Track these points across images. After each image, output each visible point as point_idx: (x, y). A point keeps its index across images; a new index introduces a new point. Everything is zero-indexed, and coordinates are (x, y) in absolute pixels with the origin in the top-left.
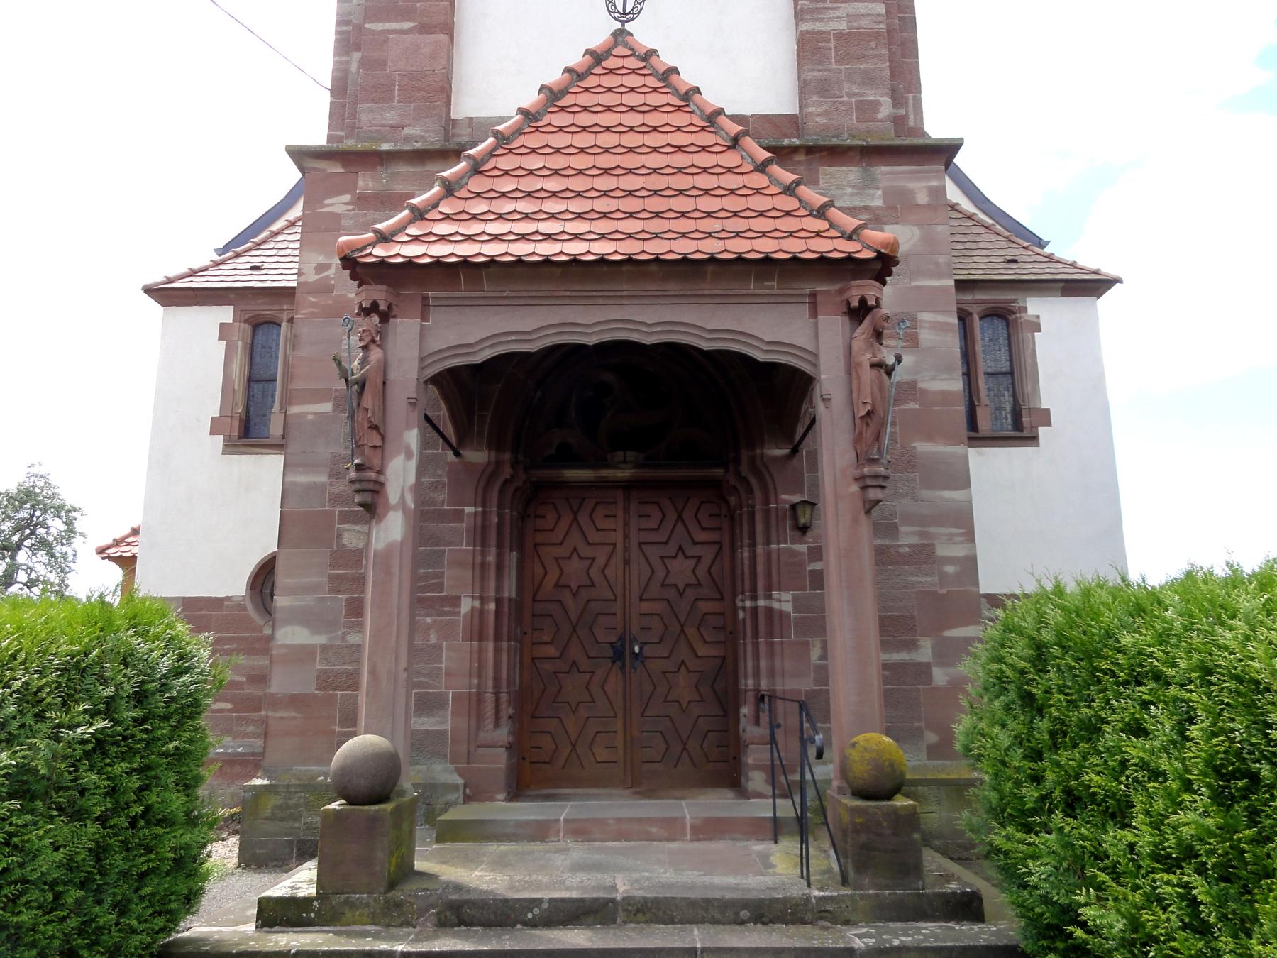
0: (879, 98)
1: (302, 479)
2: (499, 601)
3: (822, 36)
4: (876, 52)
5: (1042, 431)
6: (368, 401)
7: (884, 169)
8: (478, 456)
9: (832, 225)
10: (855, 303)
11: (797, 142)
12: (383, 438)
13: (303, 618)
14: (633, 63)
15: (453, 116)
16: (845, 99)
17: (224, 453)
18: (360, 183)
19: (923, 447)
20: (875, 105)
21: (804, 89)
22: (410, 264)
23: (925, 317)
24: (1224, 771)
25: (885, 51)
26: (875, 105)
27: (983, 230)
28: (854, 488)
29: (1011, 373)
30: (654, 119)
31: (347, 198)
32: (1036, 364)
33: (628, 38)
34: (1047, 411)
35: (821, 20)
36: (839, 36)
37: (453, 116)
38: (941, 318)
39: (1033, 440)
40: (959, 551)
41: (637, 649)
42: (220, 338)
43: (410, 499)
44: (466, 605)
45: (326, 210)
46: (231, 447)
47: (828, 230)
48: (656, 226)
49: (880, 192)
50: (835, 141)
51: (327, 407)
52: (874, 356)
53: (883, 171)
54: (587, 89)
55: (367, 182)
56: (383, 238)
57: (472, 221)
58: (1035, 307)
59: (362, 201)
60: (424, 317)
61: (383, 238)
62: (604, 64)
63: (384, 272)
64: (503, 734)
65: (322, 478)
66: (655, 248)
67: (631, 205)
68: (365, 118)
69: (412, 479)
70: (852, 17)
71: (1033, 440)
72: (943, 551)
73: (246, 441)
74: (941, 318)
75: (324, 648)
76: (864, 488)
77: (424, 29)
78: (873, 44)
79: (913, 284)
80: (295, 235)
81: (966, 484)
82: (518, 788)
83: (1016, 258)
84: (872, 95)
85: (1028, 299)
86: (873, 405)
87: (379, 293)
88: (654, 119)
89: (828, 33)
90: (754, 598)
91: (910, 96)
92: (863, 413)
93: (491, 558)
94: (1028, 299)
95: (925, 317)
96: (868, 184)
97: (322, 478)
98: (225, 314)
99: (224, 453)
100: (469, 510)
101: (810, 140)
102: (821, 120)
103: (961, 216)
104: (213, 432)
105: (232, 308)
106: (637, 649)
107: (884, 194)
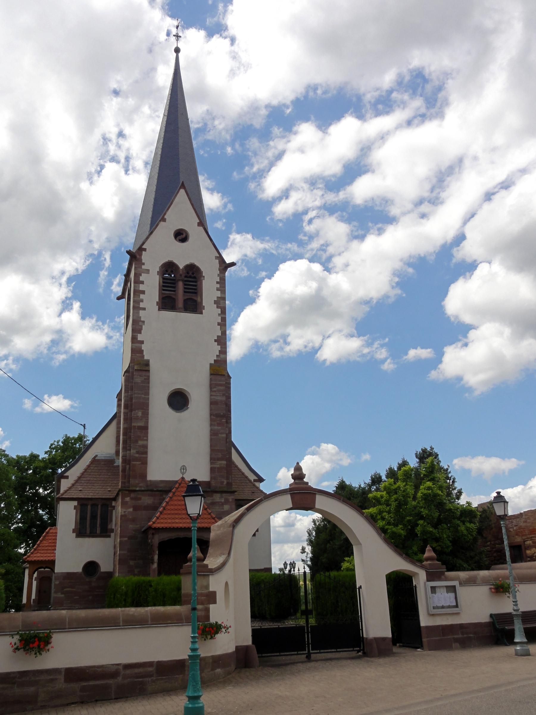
3: (215, 468)
7: (225, 494)
17: (76, 538)
18: (132, 495)
20: (223, 482)
22: (159, 528)
24: (13, 522)
31: (129, 498)
36: (218, 468)
42: (74, 509)
49: (223, 499)
51: (126, 539)
53: (224, 495)
55: (133, 495)
59: (132, 499)
61: (154, 523)
68: (132, 481)
77: (143, 463)
80: (305, 655)
89: (216, 467)
91: (230, 476)
98: (75, 503)
99: (76, 538)
102: (214, 485)
103: (244, 477)
104: (73, 532)
105: (77, 502)
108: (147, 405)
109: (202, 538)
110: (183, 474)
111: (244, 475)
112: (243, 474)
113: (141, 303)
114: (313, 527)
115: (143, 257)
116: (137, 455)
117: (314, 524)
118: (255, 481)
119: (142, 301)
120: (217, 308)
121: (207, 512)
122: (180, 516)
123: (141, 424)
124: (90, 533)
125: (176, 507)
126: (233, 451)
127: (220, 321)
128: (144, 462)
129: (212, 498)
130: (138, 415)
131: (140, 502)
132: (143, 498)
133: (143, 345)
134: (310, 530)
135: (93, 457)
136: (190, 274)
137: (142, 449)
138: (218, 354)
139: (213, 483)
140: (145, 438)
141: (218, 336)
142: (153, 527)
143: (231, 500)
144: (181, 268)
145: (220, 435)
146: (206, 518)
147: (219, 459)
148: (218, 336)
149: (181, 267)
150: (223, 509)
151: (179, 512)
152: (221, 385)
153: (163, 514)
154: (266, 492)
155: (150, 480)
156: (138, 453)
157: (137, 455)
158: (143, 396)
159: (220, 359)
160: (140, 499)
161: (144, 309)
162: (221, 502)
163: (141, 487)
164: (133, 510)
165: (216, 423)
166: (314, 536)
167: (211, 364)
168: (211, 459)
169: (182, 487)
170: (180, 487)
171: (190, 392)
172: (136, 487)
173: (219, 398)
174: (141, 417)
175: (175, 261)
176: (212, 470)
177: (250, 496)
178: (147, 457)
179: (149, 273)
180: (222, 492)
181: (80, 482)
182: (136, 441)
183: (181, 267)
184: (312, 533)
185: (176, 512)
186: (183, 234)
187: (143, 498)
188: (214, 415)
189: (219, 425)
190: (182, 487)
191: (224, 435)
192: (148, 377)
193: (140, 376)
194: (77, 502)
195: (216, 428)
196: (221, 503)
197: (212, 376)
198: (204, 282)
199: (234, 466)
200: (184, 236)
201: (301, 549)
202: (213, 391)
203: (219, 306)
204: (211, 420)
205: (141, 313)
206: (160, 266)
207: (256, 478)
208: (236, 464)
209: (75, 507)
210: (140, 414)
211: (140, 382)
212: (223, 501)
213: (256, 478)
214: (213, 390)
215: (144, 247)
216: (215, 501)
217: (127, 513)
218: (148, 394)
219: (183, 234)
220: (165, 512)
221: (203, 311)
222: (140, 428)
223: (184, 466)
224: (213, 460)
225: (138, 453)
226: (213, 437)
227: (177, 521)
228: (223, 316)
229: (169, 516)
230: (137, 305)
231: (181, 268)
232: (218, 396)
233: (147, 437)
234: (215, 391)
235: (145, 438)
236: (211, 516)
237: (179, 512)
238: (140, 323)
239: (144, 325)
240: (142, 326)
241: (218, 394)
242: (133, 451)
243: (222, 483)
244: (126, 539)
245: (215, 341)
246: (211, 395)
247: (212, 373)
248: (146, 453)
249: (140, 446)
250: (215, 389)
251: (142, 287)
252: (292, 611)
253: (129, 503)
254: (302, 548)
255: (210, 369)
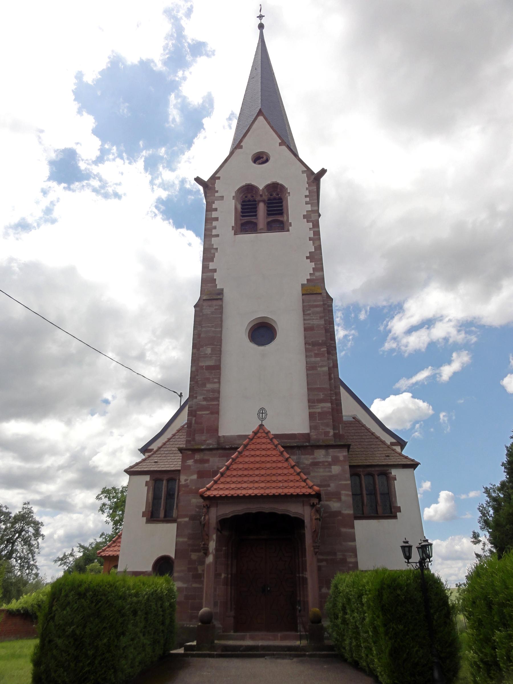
0: (330, 430)
1: (181, 540)
2: (231, 574)
4: (329, 417)
5: (398, 514)
6: (206, 529)
8: (226, 533)
9: (307, 484)
10: (312, 504)
11: (307, 444)
12: (208, 537)
13: (180, 579)
14: (264, 435)
15: (219, 435)
16: (321, 430)
18: (196, 456)
19: (343, 530)
20: (329, 432)
21: (311, 428)
22: (215, 497)
23: (343, 492)
25: (331, 417)
26: (329, 432)
27: (380, 443)
28: (312, 548)
29: (388, 494)
30: (269, 453)
31: (192, 461)
32: (395, 491)
33: (263, 427)
34: (400, 507)
35: (314, 408)
36: (319, 413)
37: (219, 435)
38: (347, 492)
39: (395, 517)
40: (352, 560)
41: (269, 589)
43: (214, 551)
44: (223, 576)
45: (187, 464)
46: (149, 521)
47: (306, 486)
48: (268, 485)
49: (330, 457)
50: (318, 444)
51: (187, 519)
52: (316, 517)
53: (331, 451)
54: (253, 443)
55: (197, 456)
56: (208, 489)
57: (228, 484)
58: (394, 472)
59: (196, 461)
60: (217, 507)
61: (208, 489)
62: (257, 435)
63: (209, 498)
64: (232, 613)
65: (186, 540)
66: (268, 492)
67: (263, 479)
68: (198, 437)
69: (214, 547)
70: (322, 408)
71: (395, 517)
72: (349, 560)
73: (152, 519)
74: (347, 492)
75: (186, 588)
76: (314, 549)
77: (212, 413)
78: (328, 415)
79: (340, 483)
81: (354, 540)
82: (236, 631)
83: (388, 455)
84: (328, 429)
85: (392, 470)
86: (315, 529)
87: (208, 503)
88: (269, 453)
89: (316, 412)
90: (299, 574)
92: (313, 531)
93: (229, 562)
94: (392, 470)
95: (343, 492)
96: (327, 454)
97: (186, 540)
98: (147, 478)
100: (224, 548)
101: (312, 442)
102: (315, 437)
103: (374, 437)
105: (149, 476)
106: (269, 589)
107: (331, 457)
108: (220, 340)
109: (288, 513)
110: (262, 420)
111: (374, 435)
112: (373, 434)
113: (213, 230)
114: (487, 501)
115: (216, 186)
116: (204, 403)
117: (487, 496)
118: (392, 444)
119: (215, 228)
120: (307, 222)
121: (295, 471)
122: (251, 479)
123: (211, 363)
124: (165, 516)
125: (246, 466)
126: (342, 390)
127: (312, 236)
128: (215, 412)
129: (312, 457)
130: (207, 352)
131: (206, 465)
132: (211, 459)
133: (215, 273)
134: (483, 507)
135: (182, 425)
136: (274, 195)
137: (211, 394)
138: (312, 272)
139: (314, 435)
140: (216, 380)
141: (310, 253)
142: (206, 496)
143: (341, 458)
144: (261, 188)
145: (319, 369)
146: (292, 481)
147: (320, 401)
148: (310, 253)
149: (261, 187)
150: (330, 471)
151: (251, 472)
152: (317, 306)
153: (225, 476)
154: (406, 455)
155: (224, 436)
156: (205, 399)
157: (204, 403)
158: (213, 329)
159: (314, 278)
160: (207, 461)
161: (218, 236)
162: (327, 462)
163: (209, 444)
164: (198, 478)
165: (313, 354)
166: (491, 516)
167: (303, 285)
168: (309, 401)
169: (259, 437)
170: (256, 437)
171: (276, 321)
172: (203, 445)
173: (316, 322)
174: (210, 354)
175: (254, 183)
176: (312, 416)
177: (383, 460)
178: (218, 405)
179: (223, 200)
180: (327, 447)
181: (159, 452)
182: (204, 385)
183: (261, 187)
184: (487, 513)
185: (246, 473)
186: (263, 158)
187: (211, 459)
188: (309, 344)
189: (316, 355)
190: (259, 437)
191: (326, 369)
192: (221, 307)
193: (210, 306)
194: (149, 476)
195: (313, 359)
196: (326, 464)
197: (304, 296)
198: (289, 198)
199: (361, 425)
200: (265, 158)
201: (472, 536)
202: (306, 315)
203: (309, 220)
204: (307, 350)
205: (214, 240)
206: (236, 190)
207: (394, 441)
208: (362, 423)
209: (147, 483)
210: (209, 351)
211: (209, 313)
212: (330, 460)
213: (394, 441)
214: (305, 313)
215: (217, 175)
216: (318, 460)
217: (188, 481)
218: (220, 325)
219: (263, 158)
220: (228, 473)
221: (290, 228)
222: (209, 368)
223: (262, 409)
224: (311, 402)
225: (205, 399)
226: (311, 372)
227: (245, 485)
228: (316, 229)
229: (234, 479)
230: (209, 233)
231: (261, 188)
232: (313, 319)
233: (219, 379)
234: (309, 314)
235: (216, 380)
236: (301, 478)
237: (251, 472)
238: (213, 251)
239: (217, 252)
240: (214, 254)
241: (313, 317)
242: (200, 398)
243: (326, 433)
244: (187, 519)
245: (307, 258)
246: (304, 320)
247: (304, 293)
248: (217, 399)
249: (208, 391)
250: (308, 312)
251: (214, 215)
252: (436, 675)
253: (192, 467)
254: (474, 535)
255: (302, 290)
